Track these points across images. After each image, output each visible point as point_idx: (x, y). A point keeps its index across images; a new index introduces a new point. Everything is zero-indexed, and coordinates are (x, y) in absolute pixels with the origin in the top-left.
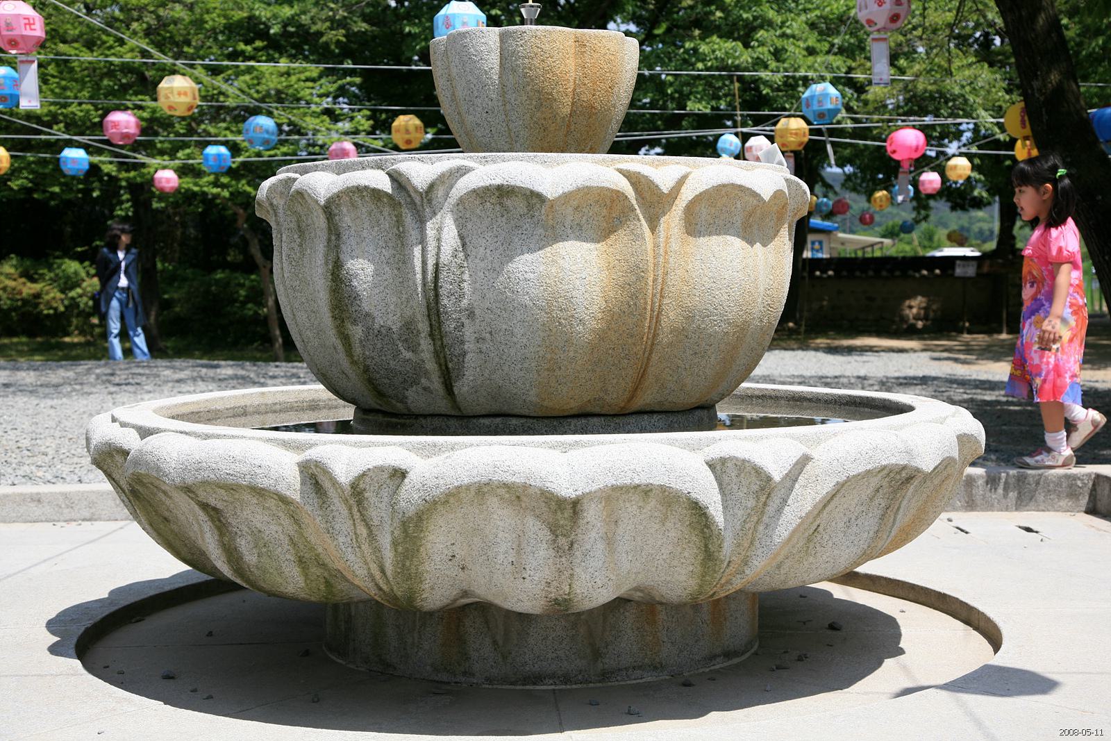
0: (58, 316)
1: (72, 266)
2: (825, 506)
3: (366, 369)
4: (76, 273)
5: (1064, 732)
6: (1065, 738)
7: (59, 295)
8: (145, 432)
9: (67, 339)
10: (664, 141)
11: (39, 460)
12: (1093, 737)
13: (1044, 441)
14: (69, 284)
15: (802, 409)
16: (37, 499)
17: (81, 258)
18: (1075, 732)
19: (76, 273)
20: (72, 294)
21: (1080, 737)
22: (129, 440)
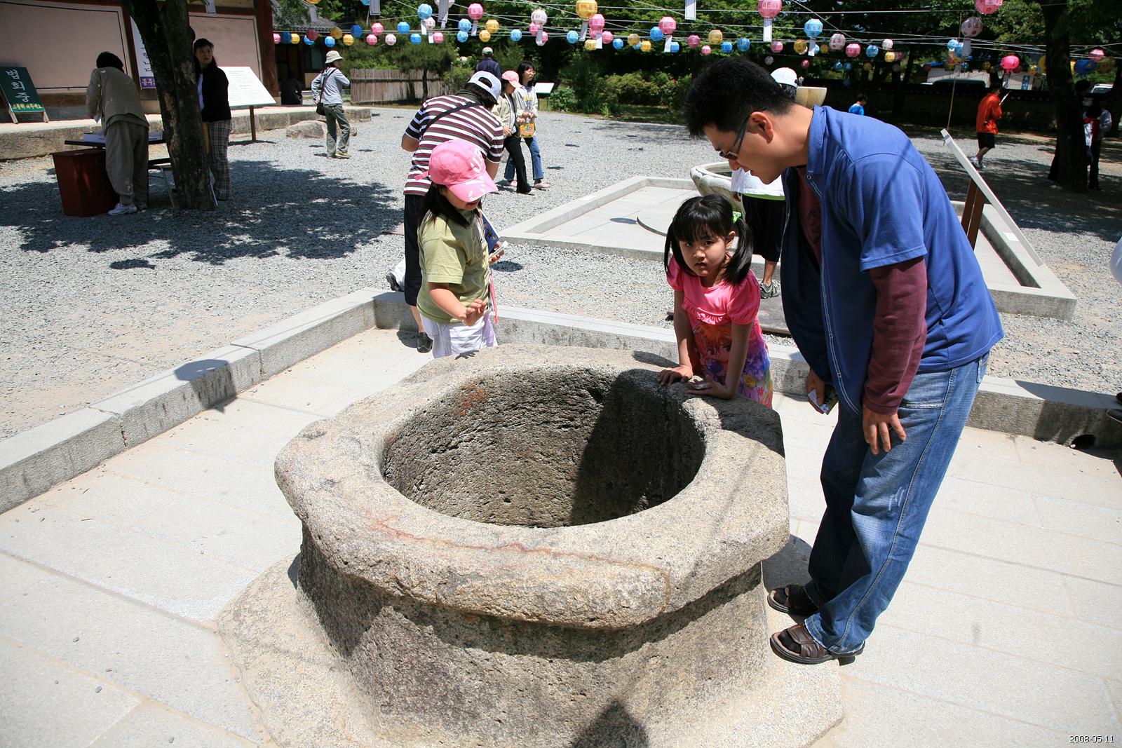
0: (656, 96)
1: (663, 75)
2: (15, 159)
3: (909, 294)
4: (665, 78)
5: (1075, 739)
6: (1076, 745)
7: (657, 88)
8: (703, 174)
9: (659, 107)
10: (833, 9)
11: (666, 169)
12: (1104, 745)
13: (185, 250)
14: (662, 83)
15: (971, 394)
16: (669, 182)
17: (667, 72)
18: (1087, 740)
19: (665, 78)
20: (662, 87)
21: (1091, 744)
22: (700, 175)
